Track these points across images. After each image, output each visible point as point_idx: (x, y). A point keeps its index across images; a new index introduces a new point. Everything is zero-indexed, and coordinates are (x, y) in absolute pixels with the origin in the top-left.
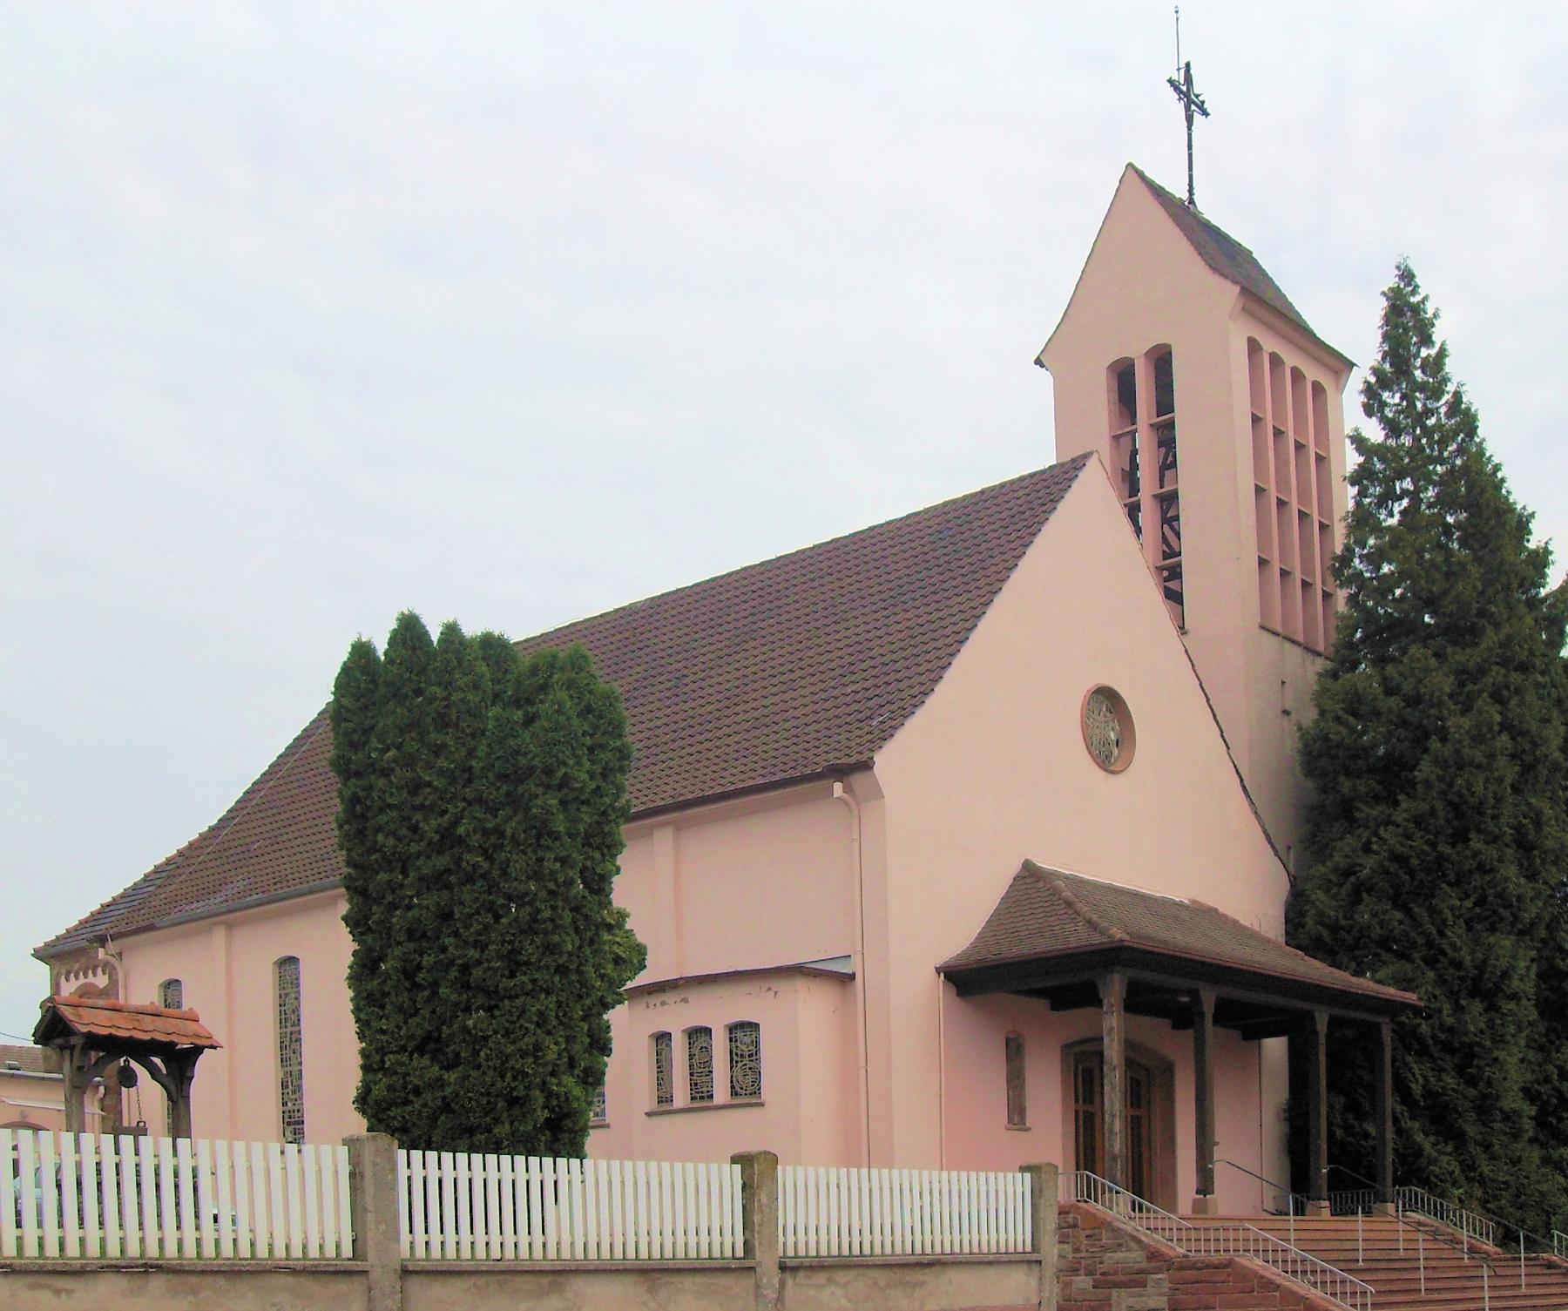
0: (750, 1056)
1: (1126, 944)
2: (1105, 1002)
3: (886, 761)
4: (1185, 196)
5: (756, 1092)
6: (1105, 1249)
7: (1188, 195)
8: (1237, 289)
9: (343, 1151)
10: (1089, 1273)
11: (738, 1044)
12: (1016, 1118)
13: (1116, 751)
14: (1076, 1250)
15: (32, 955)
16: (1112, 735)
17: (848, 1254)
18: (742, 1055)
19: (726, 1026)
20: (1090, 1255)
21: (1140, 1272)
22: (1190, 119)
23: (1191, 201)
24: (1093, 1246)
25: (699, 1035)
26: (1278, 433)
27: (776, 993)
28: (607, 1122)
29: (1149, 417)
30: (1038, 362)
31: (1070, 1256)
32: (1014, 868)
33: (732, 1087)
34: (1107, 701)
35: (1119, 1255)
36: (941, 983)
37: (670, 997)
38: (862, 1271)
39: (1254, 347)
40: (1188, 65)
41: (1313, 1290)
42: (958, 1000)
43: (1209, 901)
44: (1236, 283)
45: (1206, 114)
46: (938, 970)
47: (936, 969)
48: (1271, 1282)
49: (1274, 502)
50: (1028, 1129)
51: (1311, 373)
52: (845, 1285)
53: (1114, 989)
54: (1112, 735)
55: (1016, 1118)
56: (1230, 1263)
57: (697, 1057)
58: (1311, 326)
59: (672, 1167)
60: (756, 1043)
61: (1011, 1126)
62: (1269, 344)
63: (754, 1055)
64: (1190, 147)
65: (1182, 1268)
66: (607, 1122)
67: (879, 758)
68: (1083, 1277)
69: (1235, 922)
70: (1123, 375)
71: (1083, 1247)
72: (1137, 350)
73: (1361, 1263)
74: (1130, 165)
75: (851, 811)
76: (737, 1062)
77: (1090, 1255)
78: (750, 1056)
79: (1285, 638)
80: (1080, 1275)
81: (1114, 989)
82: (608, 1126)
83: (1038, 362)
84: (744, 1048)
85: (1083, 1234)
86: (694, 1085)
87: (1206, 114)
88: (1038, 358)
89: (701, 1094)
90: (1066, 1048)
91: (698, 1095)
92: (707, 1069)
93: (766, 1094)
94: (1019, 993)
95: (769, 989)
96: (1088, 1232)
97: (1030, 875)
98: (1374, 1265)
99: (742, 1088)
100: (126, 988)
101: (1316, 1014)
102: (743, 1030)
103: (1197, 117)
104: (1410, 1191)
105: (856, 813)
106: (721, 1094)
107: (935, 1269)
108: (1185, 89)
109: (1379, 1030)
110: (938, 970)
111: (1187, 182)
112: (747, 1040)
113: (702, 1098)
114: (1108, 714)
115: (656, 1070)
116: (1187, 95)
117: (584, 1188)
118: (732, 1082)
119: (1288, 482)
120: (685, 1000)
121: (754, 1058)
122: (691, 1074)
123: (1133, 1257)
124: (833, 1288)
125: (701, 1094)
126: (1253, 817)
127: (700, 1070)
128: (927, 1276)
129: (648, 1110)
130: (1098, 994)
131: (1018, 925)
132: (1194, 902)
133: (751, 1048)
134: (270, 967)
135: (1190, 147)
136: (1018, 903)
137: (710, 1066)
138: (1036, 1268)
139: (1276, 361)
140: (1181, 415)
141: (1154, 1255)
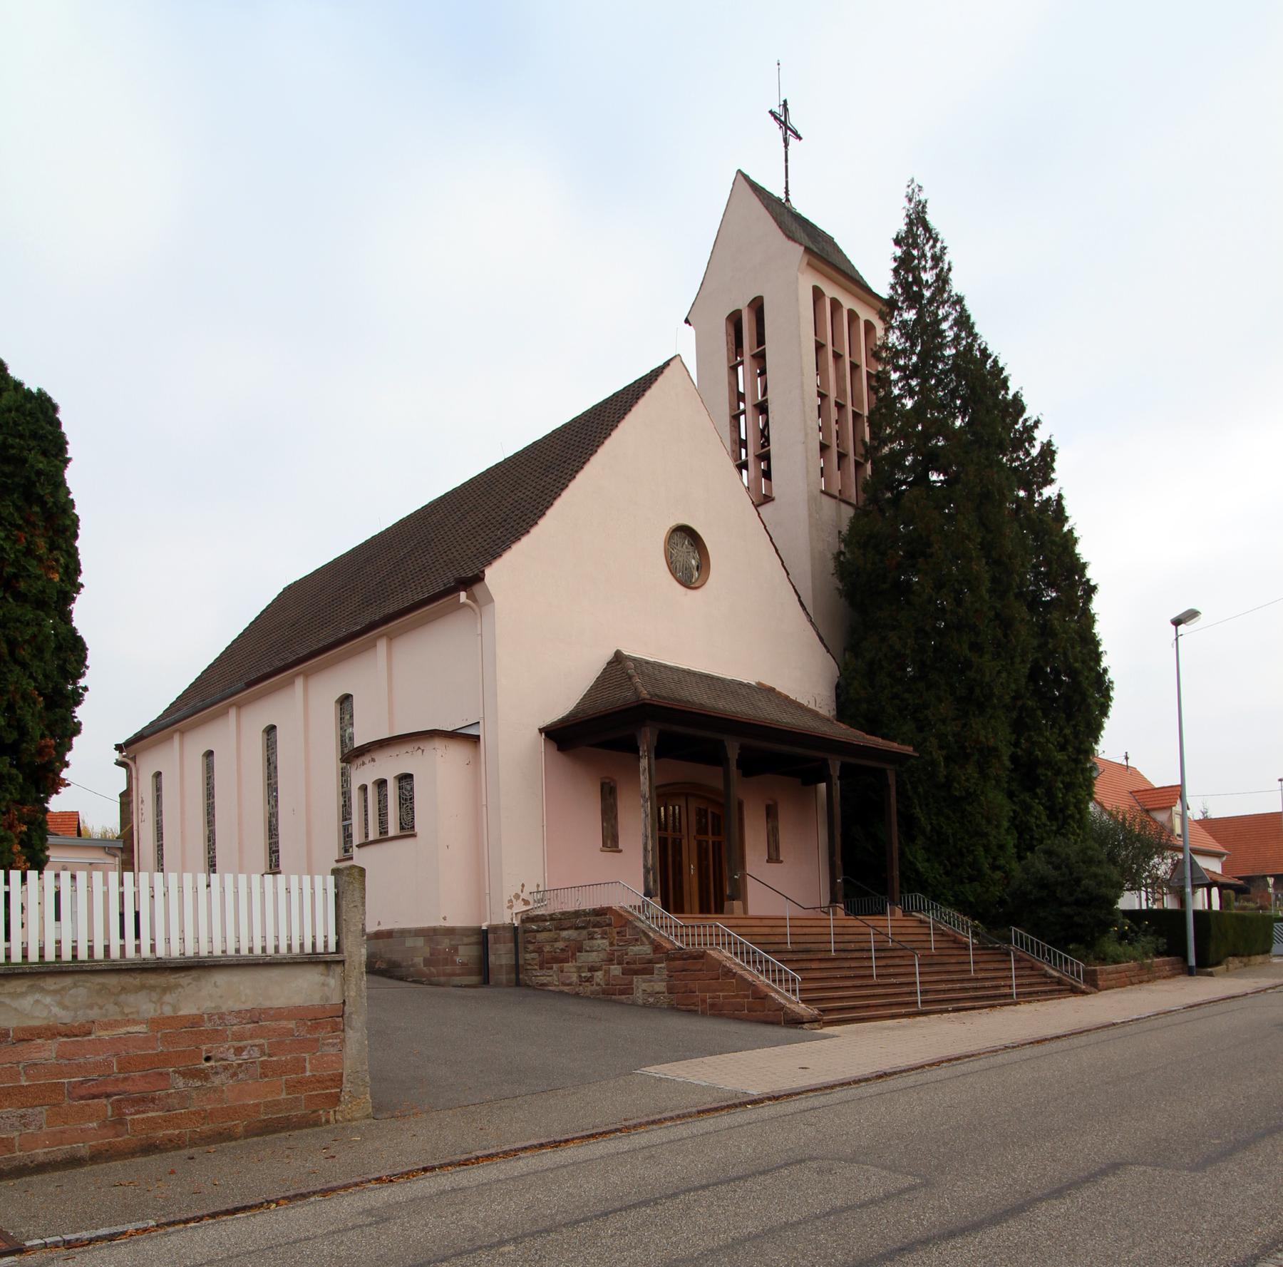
1: (646, 701)
2: (641, 749)
3: (495, 574)
4: (783, 196)
6: (628, 943)
7: (784, 195)
8: (802, 249)
9: (331, 879)
12: (609, 843)
13: (696, 574)
14: (611, 944)
16: (693, 562)
17: (310, 951)
19: (395, 777)
20: (619, 948)
21: (650, 961)
23: (788, 200)
24: (621, 941)
25: (381, 784)
26: (837, 356)
27: (423, 751)
29: (751, 350)
30: (687, 321)
32: (608, 655)
33: (401, 823)
34: (686, 536)
35: (637, 948)
37: (366, 759)
38: (82, 977)
39: (818, 294)
41: (762, 978)
42: (558, 753)
43: (768, 682)
44: (801, 244)
45: (799, 138)
46: (541, 731)
48: (730, 970)
49: (833, 404)
50: (620, 851)
52: (56, 992)
53: (647, 740)
54: (693, 562)
55: (609, 842)
56: (702, 956)
58: (870, 285)
59: (90, 878)
61: (605, 849)
62: (830, 291)
64: (786, 160)
65: (674, 959)
67: (490, 573)
69: (787, 697)
70: (735, 320)
71: (615, 942)
72: (742, 304)
73: (833, 954)
74: (739, 171)
75: (476, 614)
77: (619, 948)
79: (840, 500)
80: (613, 965)
81: (647, 740)
83: (687, 321)
84: (406, 793)
85: (615, 930)
87: (799, 138)
94: (592, 746)
95: (419, 748)
96: (618, 929)
97: (618, 658)
98: (843, 955)
100: (137, 779)
101: (830, 762)
102: (405, 779)
103: (792, 140)
104: (916, 896)
105: (479, 615)
106: (393, 830)
107: (194, 974)
108: (782, 119)
110: (541, 731)
111: (785, 186)
112: (409, 788)
114: (690, 546)
116: (787, 128)
117: (209, 895)
119: (845, 391)
120: (373, 760)
122: (380, 815)
123: (644, 949)
124: (38, 996)
126: (809, 624)
128: (184, 979)
130: (636, 743)
132: (759, 684)
134: (201, 758)
135: (786, 160)
138: (338, 969)
139: (836, 304)
140: (769, 347)
141: (657, 947)
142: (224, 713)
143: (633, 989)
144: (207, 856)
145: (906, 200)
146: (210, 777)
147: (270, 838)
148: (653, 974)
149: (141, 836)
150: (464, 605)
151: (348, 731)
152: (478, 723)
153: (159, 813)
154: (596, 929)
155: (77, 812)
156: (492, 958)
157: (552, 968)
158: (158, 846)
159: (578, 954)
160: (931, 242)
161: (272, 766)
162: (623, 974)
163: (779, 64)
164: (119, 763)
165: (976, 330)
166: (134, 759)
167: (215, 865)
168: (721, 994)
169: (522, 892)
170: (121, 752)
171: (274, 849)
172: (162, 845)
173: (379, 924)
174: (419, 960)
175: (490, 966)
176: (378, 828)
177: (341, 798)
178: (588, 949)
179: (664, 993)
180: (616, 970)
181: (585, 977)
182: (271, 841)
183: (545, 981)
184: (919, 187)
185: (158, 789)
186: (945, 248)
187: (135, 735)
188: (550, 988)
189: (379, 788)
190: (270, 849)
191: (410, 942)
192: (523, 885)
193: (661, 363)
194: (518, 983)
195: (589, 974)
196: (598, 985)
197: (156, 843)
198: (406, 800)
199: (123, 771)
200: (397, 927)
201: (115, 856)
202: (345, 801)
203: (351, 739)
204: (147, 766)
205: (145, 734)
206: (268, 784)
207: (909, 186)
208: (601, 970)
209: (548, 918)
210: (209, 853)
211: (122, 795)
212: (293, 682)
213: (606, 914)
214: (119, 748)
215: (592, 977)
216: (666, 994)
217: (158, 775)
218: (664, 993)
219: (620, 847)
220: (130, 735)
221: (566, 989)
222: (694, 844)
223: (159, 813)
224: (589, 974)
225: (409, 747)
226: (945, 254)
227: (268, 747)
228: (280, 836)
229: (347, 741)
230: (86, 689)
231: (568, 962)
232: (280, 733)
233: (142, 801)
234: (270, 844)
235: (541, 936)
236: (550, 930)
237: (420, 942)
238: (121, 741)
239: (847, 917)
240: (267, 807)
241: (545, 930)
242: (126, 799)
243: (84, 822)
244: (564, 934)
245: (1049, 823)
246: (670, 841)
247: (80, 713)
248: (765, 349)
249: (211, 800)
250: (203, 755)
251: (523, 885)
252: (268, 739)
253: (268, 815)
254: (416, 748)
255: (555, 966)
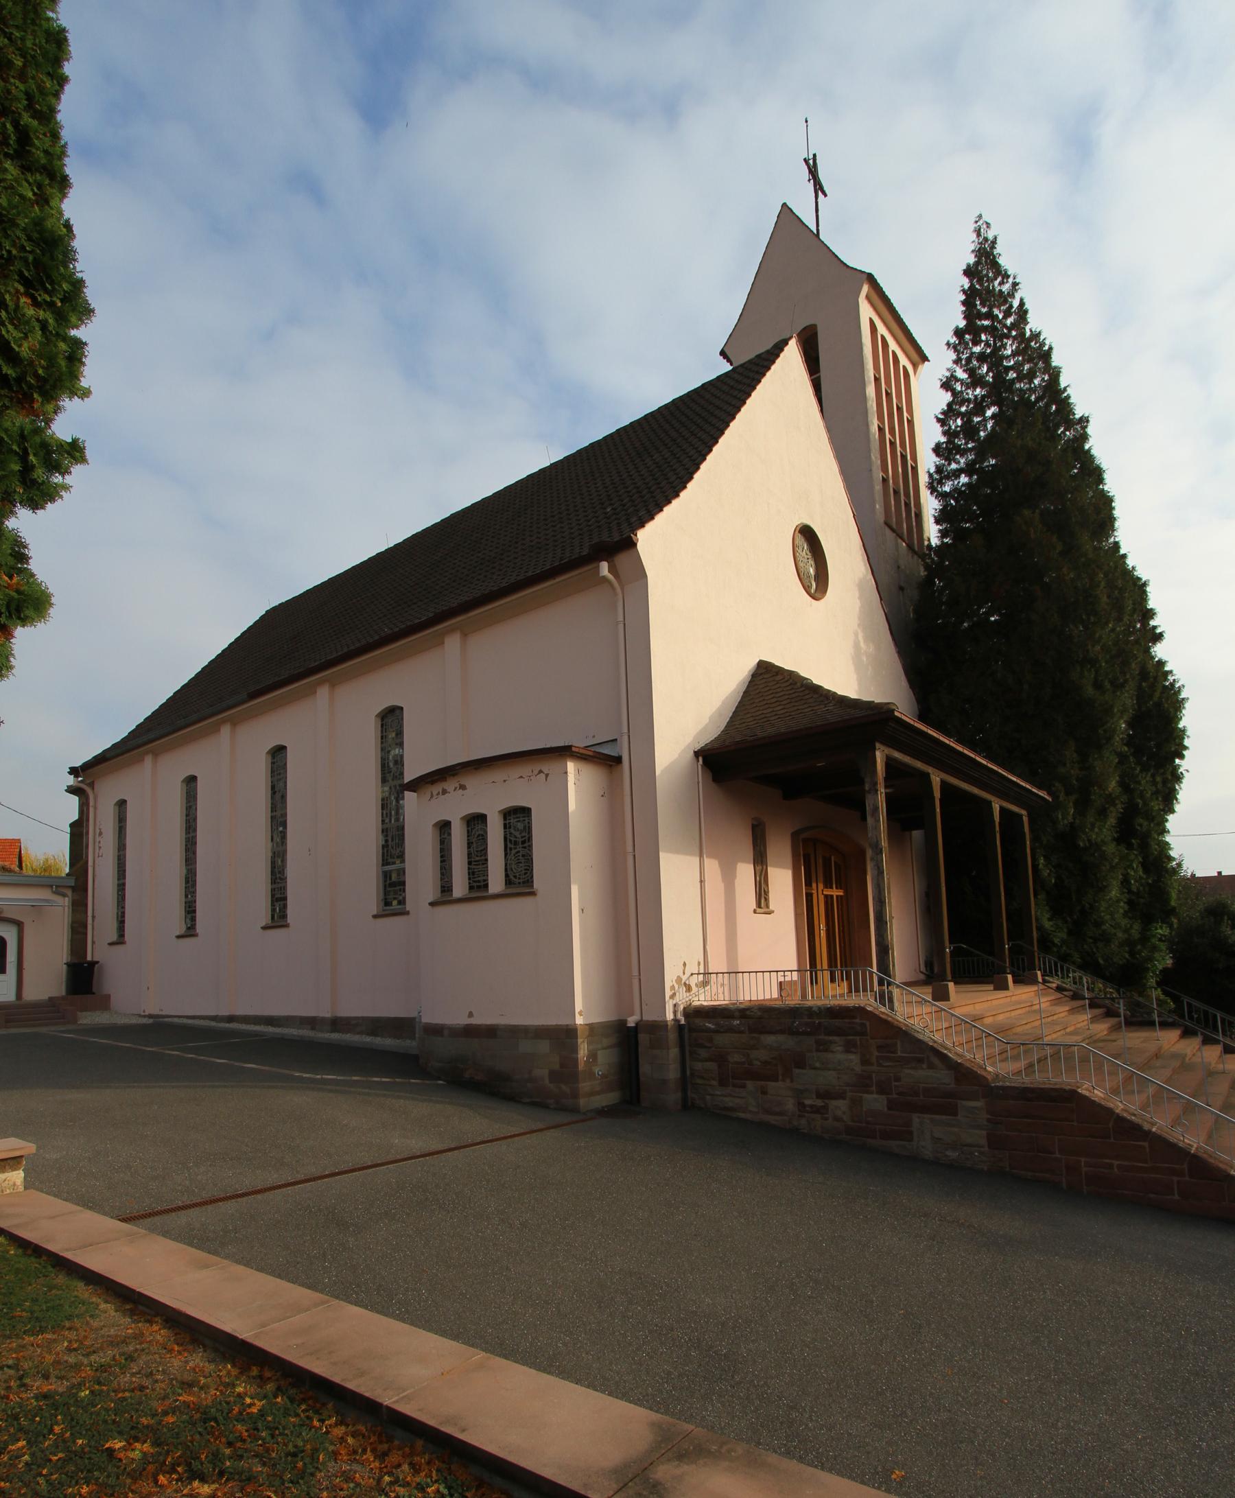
0: (523, 842)
5: (529, 882)
10: (881, 1091)
11: (512, 831)
14: (865, 1062)
15: (66, 791)
18: (515, 842)
19: (500, 812)
22: (817, 197)
27: (547, 775)
28: (407, 909)
31: (858, 1069)
32: (749, 665)
33: (507, 876)
36: (700, 767)
37: (450, 785)
40: (815, 155)
45: (825, 195)
47: (695, 752)
51: (904, 361)
57: (475, 845)
60: (528, 829)
61: (759, 910)
63: (527, 841)
66: (407, 909)
68: (875, 1096)
76: (511, 849)
78: (523, 842)
80: (872, 1093)
82: (408, 913)
84: (517, 834)
86: (471, 873)
88: (722, 349)
89: (478, 885)
90: (795, 836)
91: (475, 884)
92: (483, 858)
93: (537, 884)
95: (541, 772)
97: (765, 674)
99: (515, 877)
100: (95, 808)
102: (518, 817)
106: (496, 883)
109: (1022, 818)
112: (520, 826)
113: (479, 887)
115: (439, 859)
118: (506, 870)
120: (463, 787)
121: (526, 845)
122: (470, 863)
125: (478, 885)
127: (477, 859)
129: (178, 934)
131: (765, 712)
133: (523, 834)
136: (761, 694)
137: (486, 854)
142: (140, 760)
143: (911, 1133)
144: (184, 899)
145: (975, 235)
146: (190, 807)
147: (273, 882)
148: (956, 1115)
149: (97, 872)
150: (605, 579)
151: (392, 753)
152: (616, 740)
153: (121, 847)
154: (836, 1038)
155: (19, 840)
156: (645, 1068)
157: (744, 1086)
158: (119, 885)
159: (797, 1071)
160: (999, 279)
161: (278, 796)
162: (889, 1108)
163: (806, 121)
164: (71, 790)
165: (1056, 361)
166: (92, 785)
167: (194, 911)
168: (1116, 1163)
169: (684, 973)
170: (77, 776)
171: (279, 896)
172: (124, 884)
173: (471, 1015)
174: (542, 1073)
175: (642, 1079)
176: (467, 881)
177: (381, 837)
178: (818, 1065)
179: (982, 1147)
180: (875, 1102)
181: (811, 1106)
182: (276, 886)
183: (731, 1104)
184: (987, 223)
185: (122, 820)
186: (1018, 284)
187: (94, 757)
188: (742, 1115)
189: (468, 826)
190: (273, 896)
191: (525, 1046)
192: (685, 964)
193: (769, 346)
194: (687, 1106)
195: (819, 1103)
196: (837, 1119)
197: (116, 882)
198: (516, 843)
199: (74, 800)
200: (503, 1023)
201: (64, 895)
202: (386, 841)
203: (399, 761)
204: (108, 792)
205: (108, 756)
206: (272, 817)
207: (976, 222)
208: (844, 1098)
209: (737, 1014)
210: (186, 896)
211: (73, 825)
212: (219, 730)
213: (854, 1017)
214: (74, 771)
215: (826, 1107)
216: (986, 1149)
217: (122, 804)
218: (982, 1147)
219: (772, 907)
220: (88, 756)
221: (772, 1119)
222: (822, 898)
223: (121, 847)
224: (819, 1103)
225: (525, 770)
226: (1016, 290)
227: (272, 772)
228: (289, 880)
229: (391, 765)
230: (75, 451)
231: (777, 1080)
232: (291, 758)
233: (100, 834)
234: (273, 890)
235: (721, 1040)
236: (741, 1032)
237: (544, 1047)
238: (78, 764)
239: (474, 895)
240: (270, 844)
241: (731, 1030)
242: (78, 831)
243: (26, 849)
244: (770, 1039)
245: (1145, 876)
246: (835, 897)
247: (49, 506)
248: (820, 377)
249: (192, 834)
250: (183, 781)
251: (685, 964)
252: (273, 763)
253: (270, 854)
254: (536, 772)
255: (750, 1085)
